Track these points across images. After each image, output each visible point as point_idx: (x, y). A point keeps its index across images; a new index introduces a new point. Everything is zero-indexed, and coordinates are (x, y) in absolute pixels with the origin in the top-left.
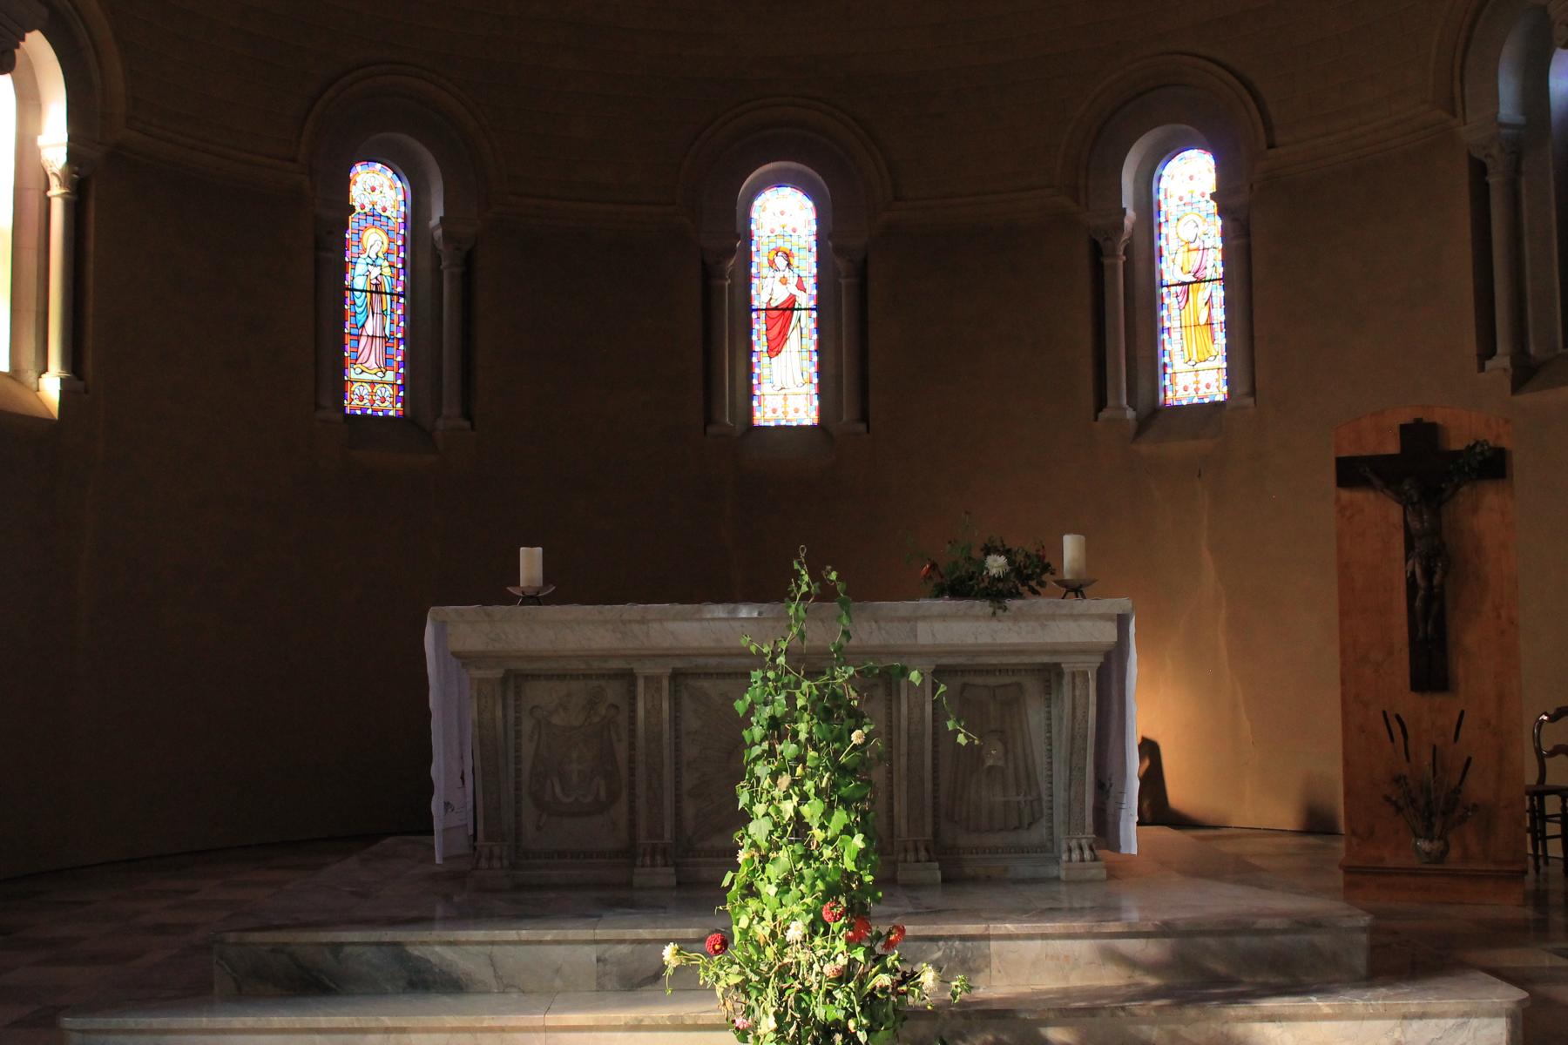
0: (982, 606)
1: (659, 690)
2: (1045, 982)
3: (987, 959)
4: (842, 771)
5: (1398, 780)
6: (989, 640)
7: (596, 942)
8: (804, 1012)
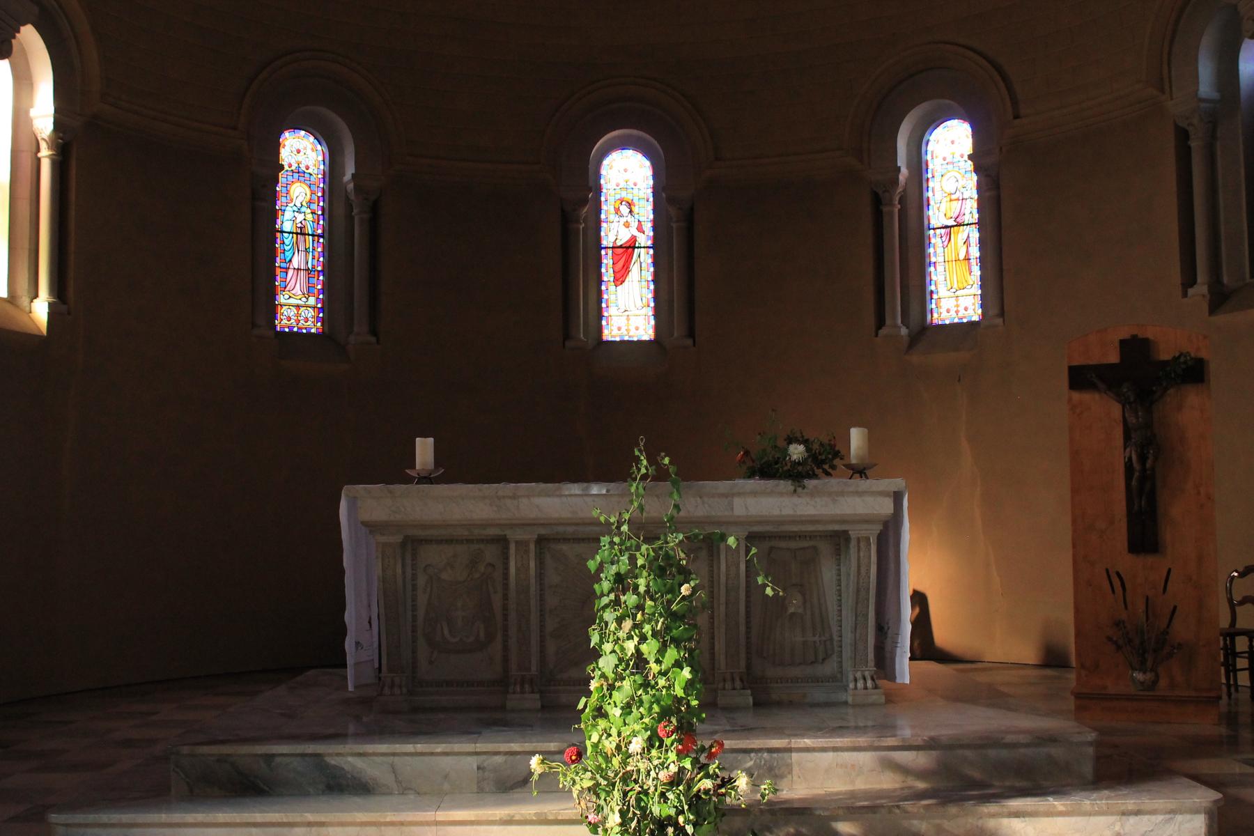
0: (785, 485)
1: (527, 552)
2: (836, 785)
3: (789, 767)
4: (673, 616)
5: (1118, 624)
6: (791, 512)
7: (477, 754)
8: (643, 809)
